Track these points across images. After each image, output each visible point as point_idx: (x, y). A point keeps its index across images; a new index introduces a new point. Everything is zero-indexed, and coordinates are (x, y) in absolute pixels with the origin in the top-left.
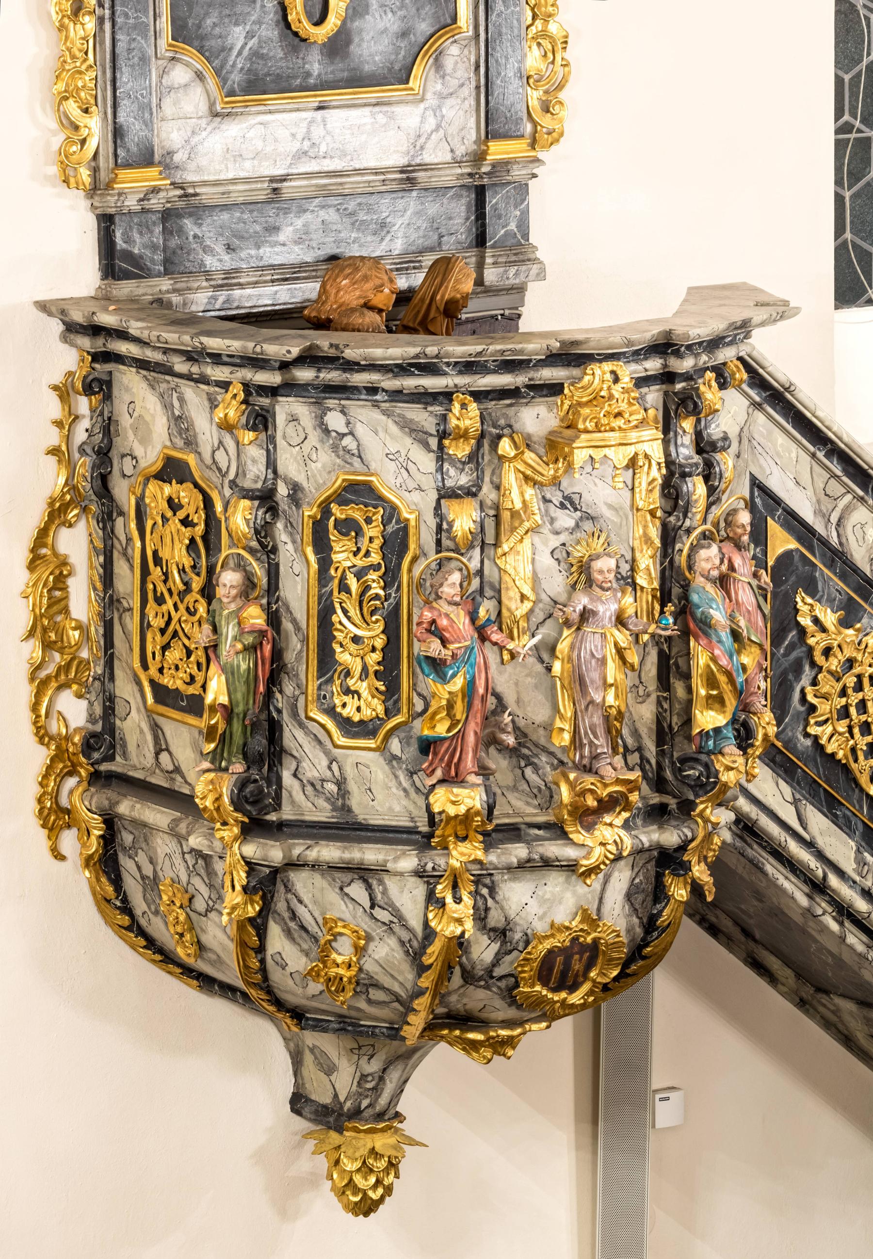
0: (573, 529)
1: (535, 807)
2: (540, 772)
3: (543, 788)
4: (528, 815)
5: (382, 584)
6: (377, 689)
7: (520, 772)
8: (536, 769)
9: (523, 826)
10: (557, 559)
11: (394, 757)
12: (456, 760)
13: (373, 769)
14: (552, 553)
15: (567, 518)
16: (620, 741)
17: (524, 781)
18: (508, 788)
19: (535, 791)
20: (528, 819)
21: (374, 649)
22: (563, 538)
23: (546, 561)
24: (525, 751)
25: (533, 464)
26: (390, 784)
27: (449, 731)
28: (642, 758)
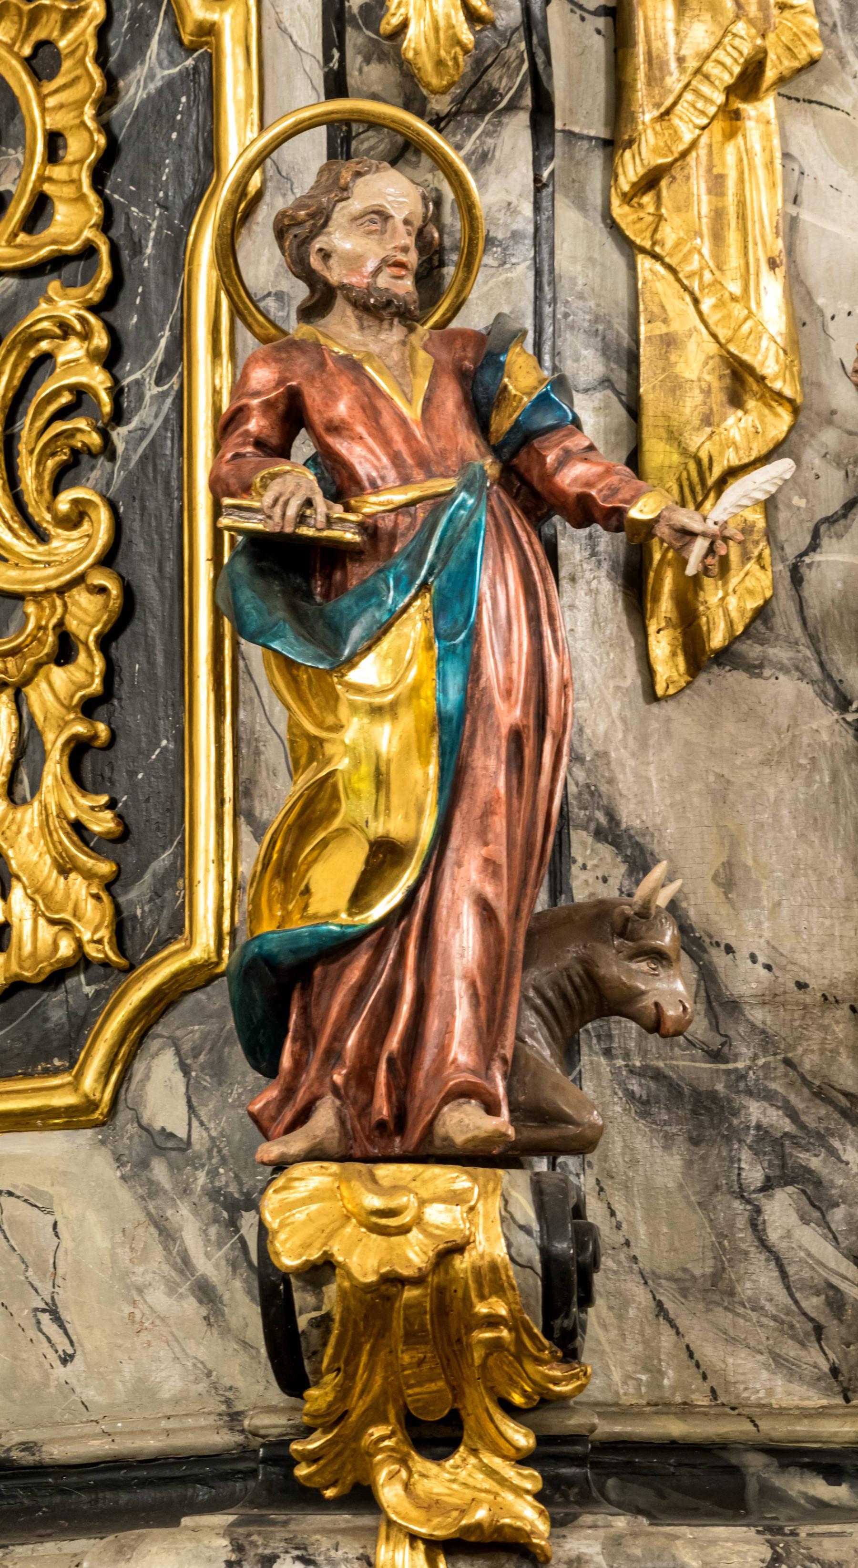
4: (781, 1413)
5: (101, 340)
6: (78, 827)
9: (755, 1462)
11: (160, 1143)
12: (394, 1042)
13: (67, 1211)
18: (685, 1285)
20: (777, 1430)
21: (65, 651)
26: (140, 1274)
27: (360, 897)
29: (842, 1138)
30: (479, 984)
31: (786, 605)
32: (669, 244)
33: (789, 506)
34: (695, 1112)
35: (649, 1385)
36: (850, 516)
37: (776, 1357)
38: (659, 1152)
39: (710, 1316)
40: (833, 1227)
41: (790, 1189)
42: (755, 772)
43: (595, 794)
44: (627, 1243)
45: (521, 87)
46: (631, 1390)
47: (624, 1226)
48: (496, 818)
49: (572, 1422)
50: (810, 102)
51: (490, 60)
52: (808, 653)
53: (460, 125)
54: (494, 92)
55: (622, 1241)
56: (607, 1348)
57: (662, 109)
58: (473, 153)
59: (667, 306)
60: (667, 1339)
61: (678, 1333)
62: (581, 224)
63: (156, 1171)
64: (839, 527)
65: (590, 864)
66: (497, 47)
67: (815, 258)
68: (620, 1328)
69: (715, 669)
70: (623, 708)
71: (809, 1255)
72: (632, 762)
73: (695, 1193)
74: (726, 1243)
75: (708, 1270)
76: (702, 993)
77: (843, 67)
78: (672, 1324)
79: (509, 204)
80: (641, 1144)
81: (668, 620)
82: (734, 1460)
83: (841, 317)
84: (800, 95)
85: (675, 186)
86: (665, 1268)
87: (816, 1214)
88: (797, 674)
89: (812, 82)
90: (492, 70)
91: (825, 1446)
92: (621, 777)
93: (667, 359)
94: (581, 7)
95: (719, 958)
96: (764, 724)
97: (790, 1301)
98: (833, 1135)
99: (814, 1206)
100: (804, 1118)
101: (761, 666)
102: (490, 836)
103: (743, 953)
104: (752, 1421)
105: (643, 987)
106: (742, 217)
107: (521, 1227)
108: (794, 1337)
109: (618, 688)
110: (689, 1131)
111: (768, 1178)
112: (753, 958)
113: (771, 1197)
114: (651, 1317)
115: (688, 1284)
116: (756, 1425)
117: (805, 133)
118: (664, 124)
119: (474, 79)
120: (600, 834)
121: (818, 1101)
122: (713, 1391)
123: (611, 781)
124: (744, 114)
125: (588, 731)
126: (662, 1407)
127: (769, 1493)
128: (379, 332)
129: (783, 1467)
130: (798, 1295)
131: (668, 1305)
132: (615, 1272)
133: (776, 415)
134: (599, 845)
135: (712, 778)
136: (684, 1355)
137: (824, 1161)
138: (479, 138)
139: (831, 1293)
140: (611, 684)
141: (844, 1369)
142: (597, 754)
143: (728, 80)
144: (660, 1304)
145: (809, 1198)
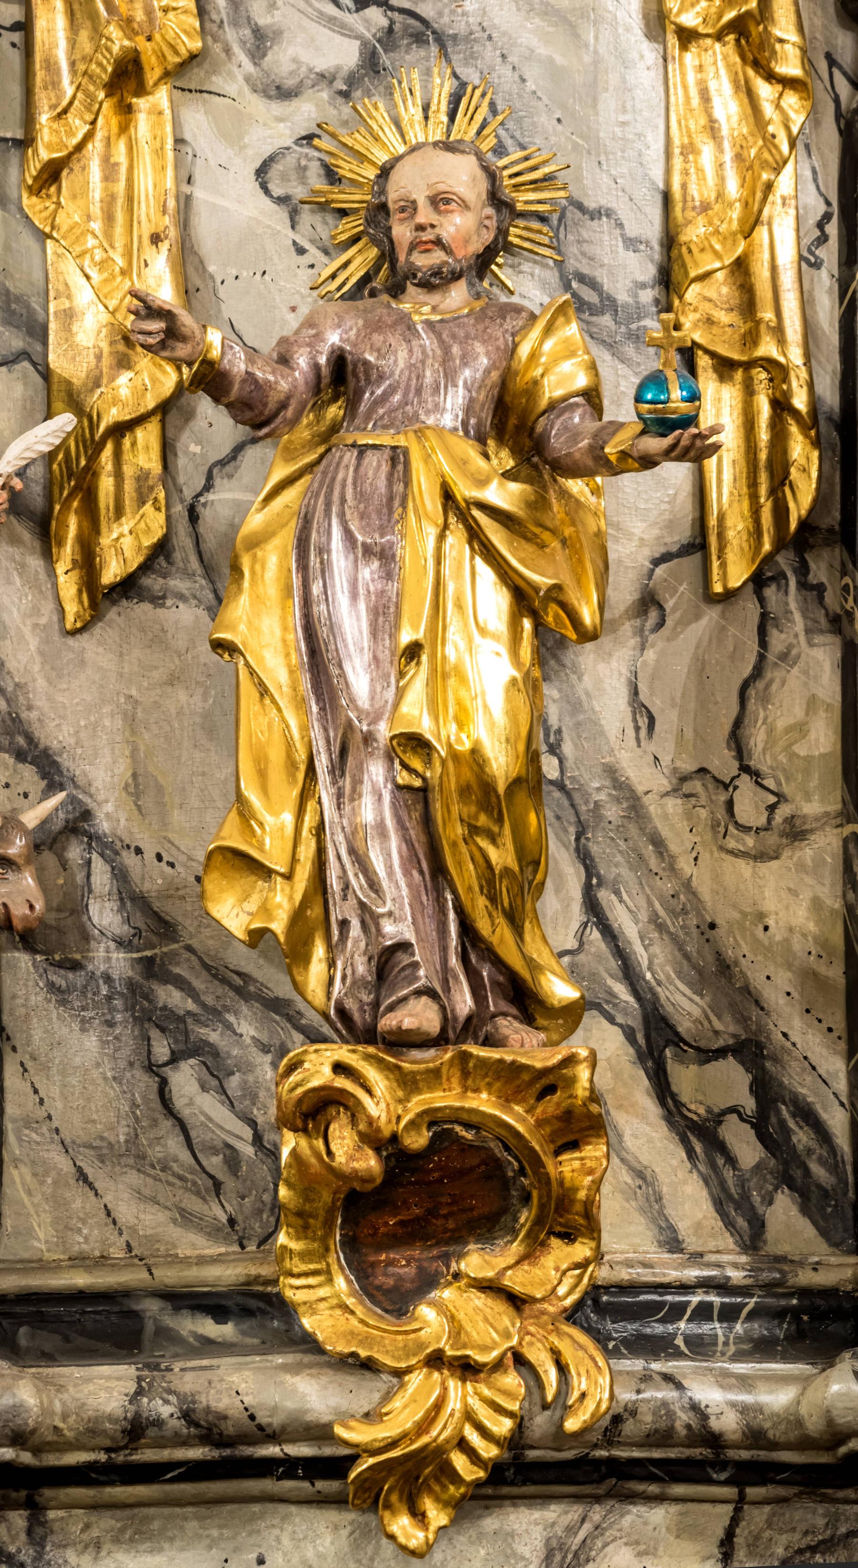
0: (352, 80)
1: (214, 1232)
2: (233, 1083)
3: (248, 1150)
7: (153, 1083)
8: (216, 1070)
9: (152, 1307)
10: (282, 200)
14: (262, 172)
15: (324, 34)
16: (449, 897)
17: (167, 1124)
18: (106, 1153)
19: (214, 1163)
20: (168, 1276)
22: (306, 111)
23: (234, 208)
24: (170, 997)
25: (680, 92)
28: (765, 1089)
29: (236, 1013)
31: (183, 540)
32: (64, 228)
33: (186, 453)
36: (239, 458)
37: (182, 1212)
40: (229, 1093)
41: (192, 1061)
42: (159, 691)
44: (50, 1117)
50: (201, 92)
52: (203, 582)
56: (32, 1211)
57: (59, 110)
59: (71, 284)
61: (96, 1194)
64: (228, 468)
67: (205, 229)
69: (124, 602)
71: (210, 1119)
77: (230, 59)
81: (74, 561)
82: (136, 1307)
83: (230, 281)
84: (193, 87)
85: (72, 176)
87: (214, 1083)
88: (195, 602)
89: (202, 74)
93: (70, 331)
95: (129, 859)
96: (167, 648)
97: (192, 1161)
98: (228, 1011)
100: (202, 998)
101: (164, 597)
103: (149, 855)
104: (149, 1270)
106: (130, 199)
108: (198, 1193)
111: (173, 1052)
112: (159, 857)
113: (177, 1069)
115: (105, 1151)
116: (151, 1274)
117: (197, 121)
118: (62, 122)
121: (216, 982)
124: (135, 108)
126: (79, 1261)
127: (165, 1335)
129: (177, 1309)
130: (200, 1156)
131: (89, 1171)
133: (164, 372)
134: (20, 765)
135: (122, 700)
136: (102, 1214)
137: (222, 1034)
139: (228, 1152)
140: (28, 622)
141: (240, 1219)
143: (105, 78)
144: (80, 1170)
145: (208, 1068)
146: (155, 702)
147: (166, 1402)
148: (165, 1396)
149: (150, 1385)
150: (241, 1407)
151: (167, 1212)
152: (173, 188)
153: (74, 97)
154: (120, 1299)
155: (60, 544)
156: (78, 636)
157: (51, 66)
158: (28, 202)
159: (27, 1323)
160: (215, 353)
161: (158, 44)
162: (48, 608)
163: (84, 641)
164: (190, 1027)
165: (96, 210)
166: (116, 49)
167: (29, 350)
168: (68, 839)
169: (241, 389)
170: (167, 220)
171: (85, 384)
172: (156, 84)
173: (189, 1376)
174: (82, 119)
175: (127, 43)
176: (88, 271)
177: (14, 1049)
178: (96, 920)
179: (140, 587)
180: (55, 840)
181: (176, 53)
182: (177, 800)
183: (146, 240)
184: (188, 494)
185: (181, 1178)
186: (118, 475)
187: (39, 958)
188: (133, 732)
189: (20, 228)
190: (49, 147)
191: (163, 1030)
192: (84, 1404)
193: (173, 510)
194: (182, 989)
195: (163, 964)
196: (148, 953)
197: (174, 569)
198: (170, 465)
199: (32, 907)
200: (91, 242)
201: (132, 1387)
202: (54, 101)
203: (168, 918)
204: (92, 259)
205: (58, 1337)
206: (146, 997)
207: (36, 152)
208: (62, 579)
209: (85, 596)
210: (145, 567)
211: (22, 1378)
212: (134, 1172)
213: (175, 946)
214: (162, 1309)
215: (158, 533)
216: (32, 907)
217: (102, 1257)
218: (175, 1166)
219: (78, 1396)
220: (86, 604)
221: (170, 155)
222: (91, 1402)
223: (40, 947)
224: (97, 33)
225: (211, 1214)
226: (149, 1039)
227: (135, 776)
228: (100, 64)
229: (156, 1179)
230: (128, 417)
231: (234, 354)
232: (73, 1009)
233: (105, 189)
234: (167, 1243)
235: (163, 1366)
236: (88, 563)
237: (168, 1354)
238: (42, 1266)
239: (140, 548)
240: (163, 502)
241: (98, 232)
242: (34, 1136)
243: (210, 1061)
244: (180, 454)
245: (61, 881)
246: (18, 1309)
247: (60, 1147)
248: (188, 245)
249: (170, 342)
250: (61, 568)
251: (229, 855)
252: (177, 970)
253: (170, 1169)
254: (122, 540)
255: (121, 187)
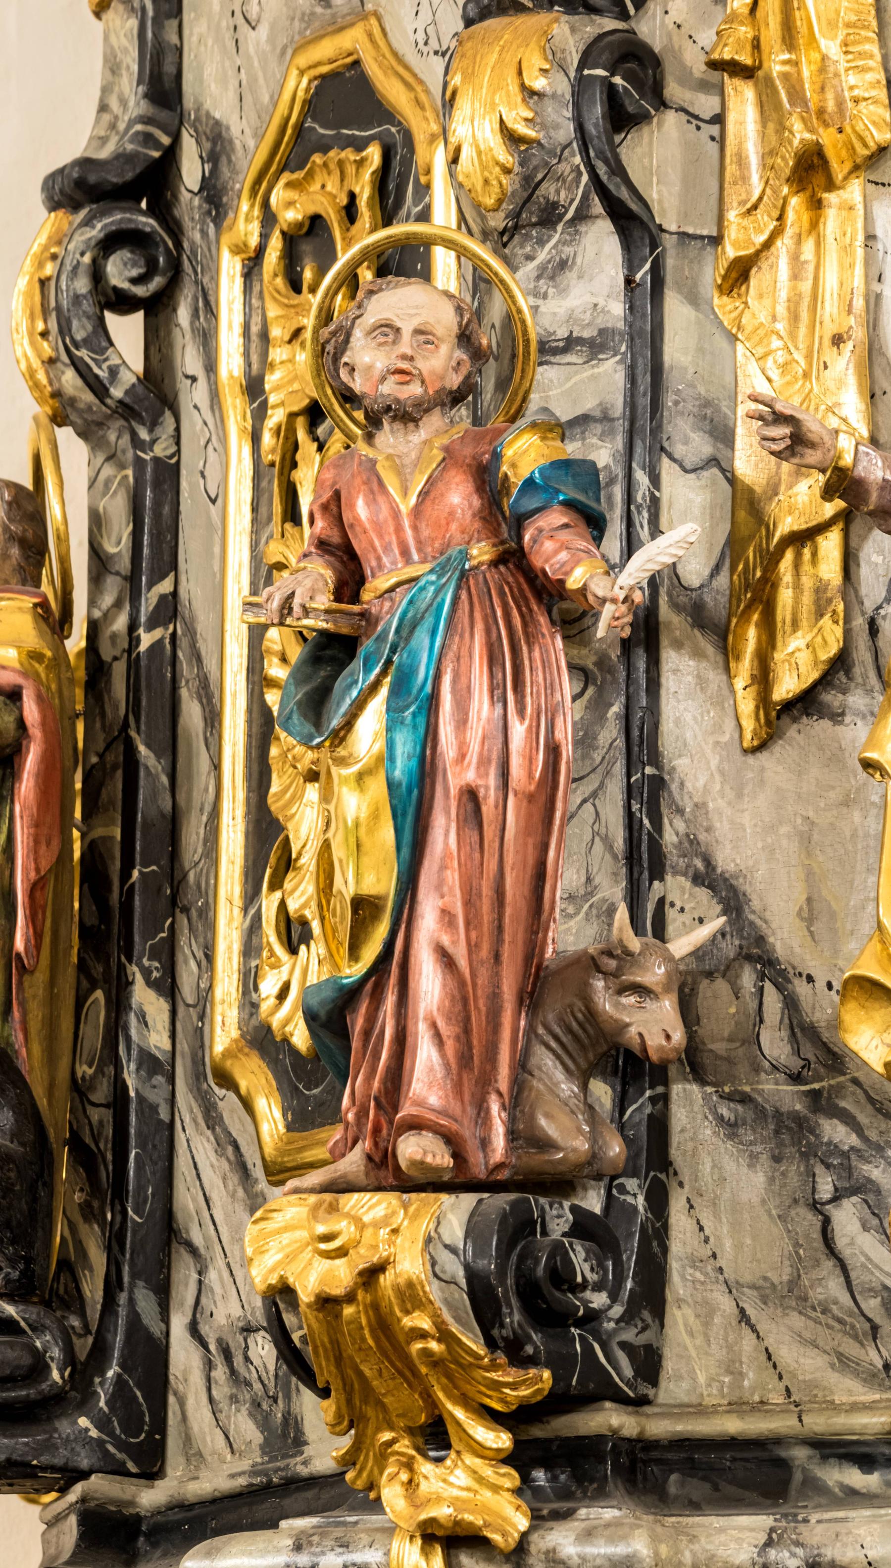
1: (870, 1378)
7: (816, 1221)
9: (800, 1454)
17: (829, 1264)
18: (766, 1292)
20: (818, 1423)
24: (835, 1132)
30: (441, 1024)
32: (749, 329)
33: (869, 562)
34: (777, 1132)
35: (731, 1386)
38: (745, 1170)
39: (787, 1321)
41: (854, 1199)
42: (835, 812)
43: (694, 842)
44: (714, 1256)
45: (585, 197)
46: (715, 1392)
47: (712, 1240)
48: (449, 872)
49: (592, 1424)
51: (540, 176)
53: (528, 237)
54: (555, 205)
55: (710, 1253)
56: (693, 1353)
57: (749, 206)
58: (549, 262)
60: (748, 1341)
61: (758, 1337)
62: (693, 318)
63: (294, 1210)
65: (687, 907)
66: (547, 163)
68: (706, 1336)
69: (805, 719)
70: (721, 762)
71: (869, 1259)
72: (728, 811)
73: (776, 1207)
74: (801, 1252)
75: (785, 1278)
76: (786, 1021)
78: (754, 1329)
79: (596, 305)
80: (729, 1166)
81: (753, 676)
82: (783, 1454)
85: (759, 275)
86: (747, 1278)
87: (875, 1222)
90: (544, 185)
91: (862, 1438)
92: (718, 825)
94: (697, 117)
95: (801, 988)
97: (851, 1304)
99: (874, 1214)
100: (867, 1133)
101: (843, 714)
102: (445, 889)
103: (820, 984)
105: (628, 1020)
107: (446, 1246)
108: (856, 1337)
109: (717, 743)
110: (771, 1149)
111: (836, 1189)
112: (830, 986)
113: (840, 1206)
114: (734, 1323)
115: (768, 1291)
116: (801, 1421)
118: (751, 218)
119: (525, 195)
120: (698, 879)
122: (787, 1389)
123: (708, 830)
124: (825, 203)
125: (689, 785)
128: (406, 434)
129: (824, 1458)
130: (858, 1297)
131: (750, 1311)
132: (703, 1283)
136: (763, 1357)
137: (884, 1171)
138: (555, 247)
140: (711, 740)
142: (696, 805)
144: (742, 1311)
145: (869, 1207)
146: (831, 824)
147: (793, 1555)
148: (793, 1548)
149: (780, 1537)
150: (865, 1561)
151: (826, 1356)
152: (862, 287)
153: (764, 192)
154: (770, 1447)
155: (738, 658)
156: (758, 754)
157: (741, 160)
158: (719, 302)
159: (678, 1470)
160: (847, 460)
161: (848, 136)
162: (729, 725)
163: (763, 757)
164: (854, 1163)
165: (781, 310)
166: (796, 142)
167: (719, 456)
168: (741, 967)
169: (880, 497)
170: (852, 321)
171: (765, 492)
172: (846, 178)
173: (820, 1528)
174: (769, 216)
175: (807, 136)
176: (770, 374)
177: (681, 1184)
178: (766, 1052)
179: (821, 704)
180: (728, 967)
181: (866, 145)
182: (849, 927)
183: (827, 341)
184: (869, 606)
185: (840, 1321)
186: (797, 586)
187: (709, 1089)
188: (809, 854)
189: (714, 330)
190: (736, 245)
191: (828, 1166)
192: (713, 1556)
193: (854, 623)
194: (847, 1124)
195: (829, 1097)
196: (816, 1086)
197: (853, 685)
198: (853, 576)
199: (668, 1037)
200: (776, 343)
201: (762, 1538)
202: (744, 197)
203: (836, 1049)
204: (775, 362)
205: (707, 1486)
206: (812, 1131)
207: (724, 252)
208: (740, 693)
209: (762, 713)
210: (825, 681)
211: (639, 1527)
212: (795, 1314)
213: (841, 1079)
214: (810, 1458)
215: (833, 649)
216: (668, 1037)
217: (762, 1402)
218: (834, 1308)
219: (708, 1547)
220: (762, 721)
221: (860, 252)
222: (721, 1552)
223: (711, 1078)
224: (782, 127)
225: (867, 1359)
226: (814, 1175)
227: (809, 900)
228: (783, 158)
229: (817, 1322)
230: (804, 527)
231: (870, 461)
232: (741, 1143)
233: (794, 288)
234: (825, 1388)
235: (800, 1518)
236: (763, 678)
237: (811, 1504)
238: (700, 1410)
239: (816, 662)
240: (842, 615)
241: (782, 333)
242: (698, 1275)
243: (871, 1198)
244: (863, 564)
245: (733, 1010)
246: (669, 1456)
247: (724, 1288)
248: (877, 346)
249: (799, 449)
250: (739, 683)
251: (868, 985)
252: (843, 1104)
253: (830, 1311)
254: (797, 654)
255: (806, 286)
